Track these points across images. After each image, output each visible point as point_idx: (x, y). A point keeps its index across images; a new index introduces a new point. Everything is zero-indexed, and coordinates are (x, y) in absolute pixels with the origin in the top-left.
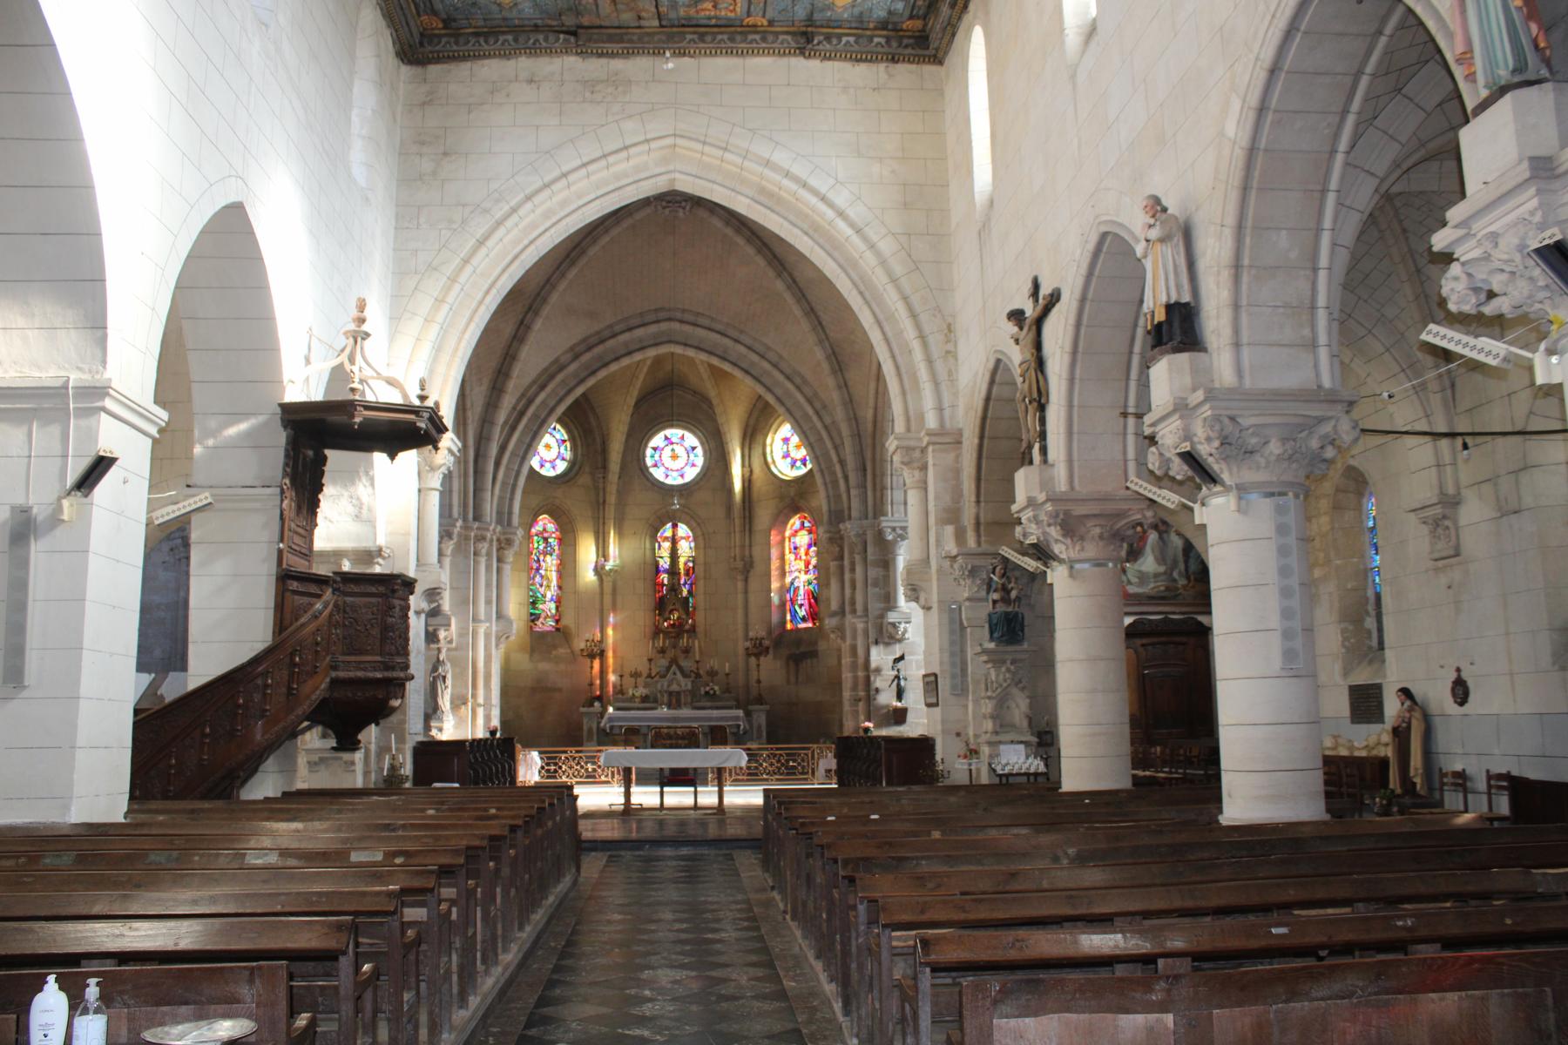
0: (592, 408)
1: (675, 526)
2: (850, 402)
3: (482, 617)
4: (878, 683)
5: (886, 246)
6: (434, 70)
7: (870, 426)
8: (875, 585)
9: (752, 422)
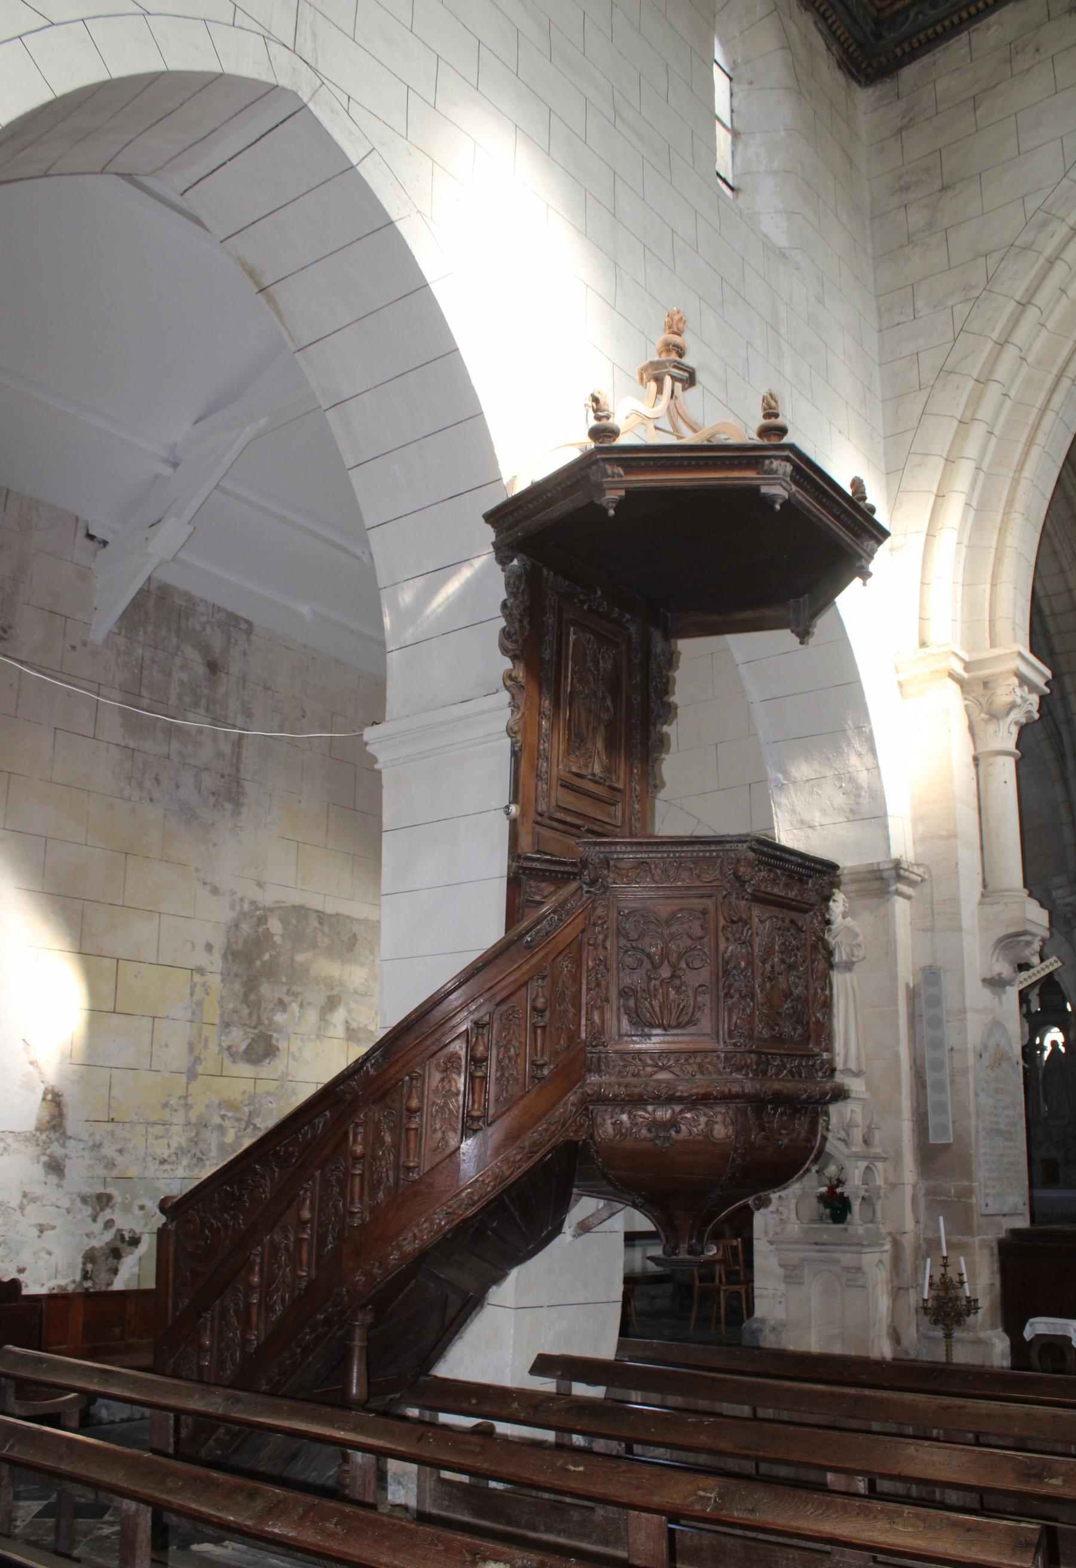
6: (908, 73)
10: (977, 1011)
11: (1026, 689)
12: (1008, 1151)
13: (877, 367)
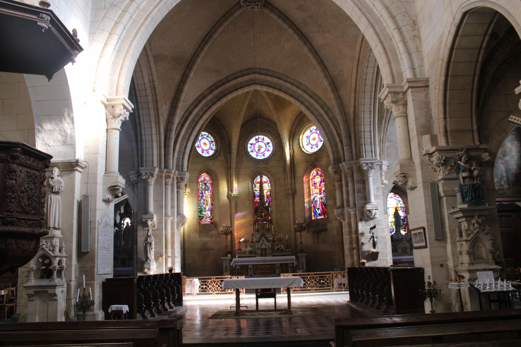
1: (261, 177)
2: (342, 106)
3: (169, 214)
4: (363, 240)
7: (352, 116)
8: (359, 192)
9: (293, 130)
10: (100, 210)
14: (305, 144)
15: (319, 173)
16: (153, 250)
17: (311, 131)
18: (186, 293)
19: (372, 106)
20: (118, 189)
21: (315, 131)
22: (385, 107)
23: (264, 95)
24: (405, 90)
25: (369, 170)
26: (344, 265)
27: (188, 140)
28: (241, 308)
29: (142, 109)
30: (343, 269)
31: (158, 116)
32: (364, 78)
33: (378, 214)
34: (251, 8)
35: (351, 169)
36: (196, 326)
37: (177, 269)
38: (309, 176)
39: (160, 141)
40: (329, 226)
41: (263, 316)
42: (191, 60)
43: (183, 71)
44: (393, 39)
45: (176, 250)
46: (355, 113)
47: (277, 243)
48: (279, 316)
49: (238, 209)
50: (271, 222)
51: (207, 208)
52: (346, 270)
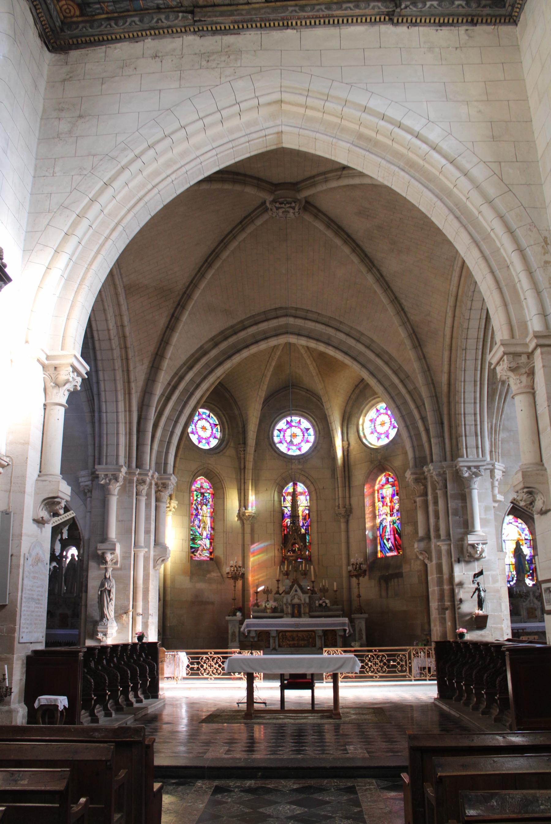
0: (236, 402)
1: (295, 484)
2: (428, 371)
3: (142, 543)
4: (461, 594)
5: (479, 173)
6: (74, 54)
7: (445, 388)
8: (456, 513)
11: (76, 374)
12: (36, 609)
13: (29, 195)
14: (367, 431)
15: (391, 480)
16: (113, 602)
17: (378, 411)
18: (165, 676)
19: (479, 372)
20: (59, 503)
21: (385, 411)
22: (499, 377)
23: (303, 351)
24: (530, 350)
25: (472, 478)
26: (430, 635)
27: (176, 422)
28: (255, 704)
29: (103, 370)
30: (427, 643)
31: (129, 382)
32: (465, 326)
33: (488, 552)
34: (283, 212)
35: (442, 475)
36: (180, 735)
37: (152, 637)
38: (374, 486)
39: (130, 423)
40: (405, 569)
41: (292, 721)
42: (185, 293)
43: (172, 311)
44: (510, 266)
45: (150, 604)
46: (449, 384)
47: (319, 595)
48: (319, 721)
49: (256, 536)
50: (309, 560)
51: (205, 534)
52: (433, 645)
